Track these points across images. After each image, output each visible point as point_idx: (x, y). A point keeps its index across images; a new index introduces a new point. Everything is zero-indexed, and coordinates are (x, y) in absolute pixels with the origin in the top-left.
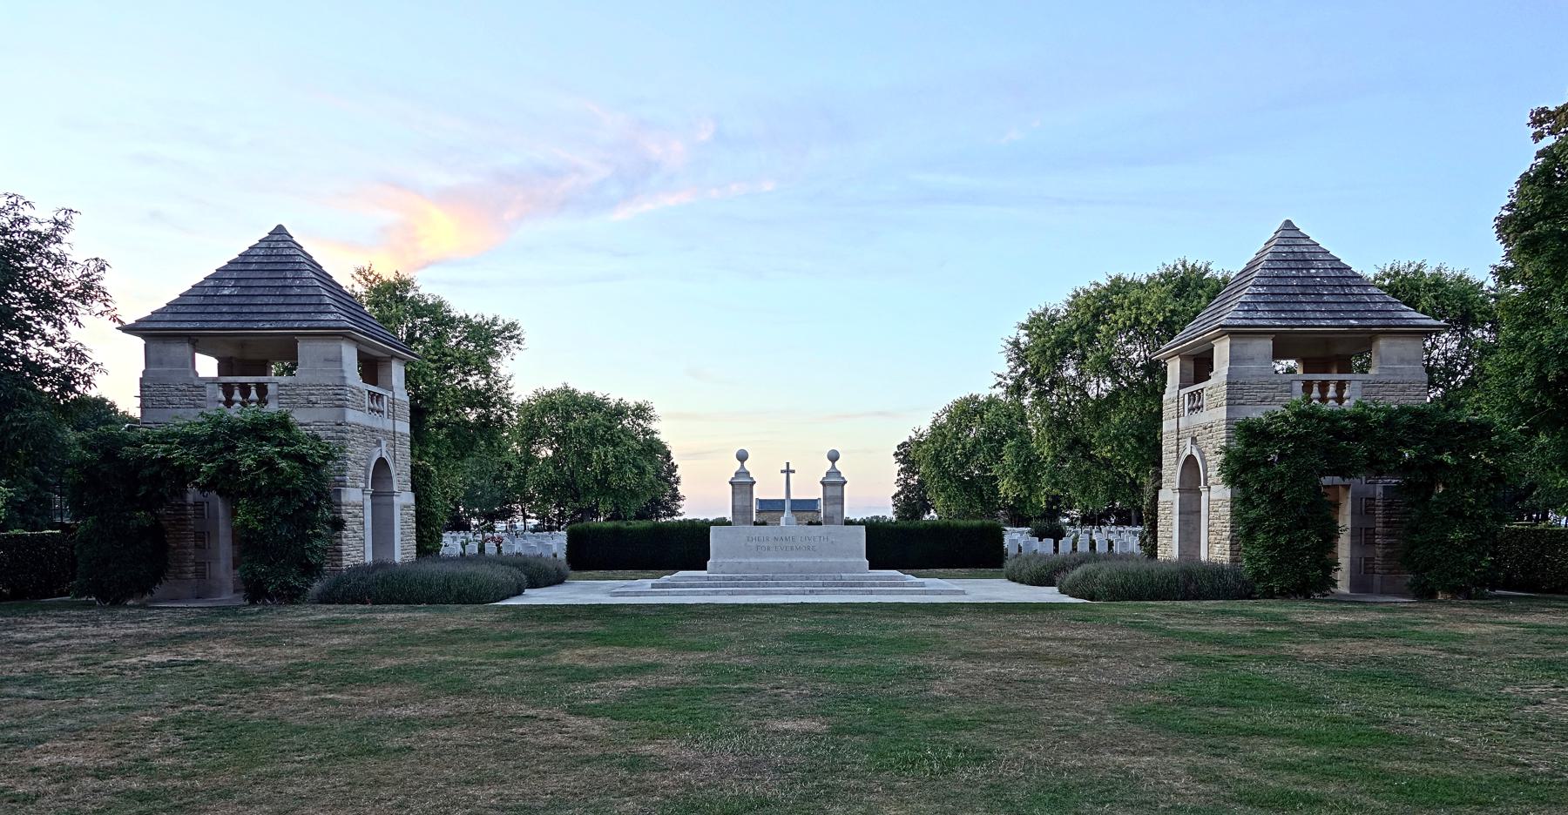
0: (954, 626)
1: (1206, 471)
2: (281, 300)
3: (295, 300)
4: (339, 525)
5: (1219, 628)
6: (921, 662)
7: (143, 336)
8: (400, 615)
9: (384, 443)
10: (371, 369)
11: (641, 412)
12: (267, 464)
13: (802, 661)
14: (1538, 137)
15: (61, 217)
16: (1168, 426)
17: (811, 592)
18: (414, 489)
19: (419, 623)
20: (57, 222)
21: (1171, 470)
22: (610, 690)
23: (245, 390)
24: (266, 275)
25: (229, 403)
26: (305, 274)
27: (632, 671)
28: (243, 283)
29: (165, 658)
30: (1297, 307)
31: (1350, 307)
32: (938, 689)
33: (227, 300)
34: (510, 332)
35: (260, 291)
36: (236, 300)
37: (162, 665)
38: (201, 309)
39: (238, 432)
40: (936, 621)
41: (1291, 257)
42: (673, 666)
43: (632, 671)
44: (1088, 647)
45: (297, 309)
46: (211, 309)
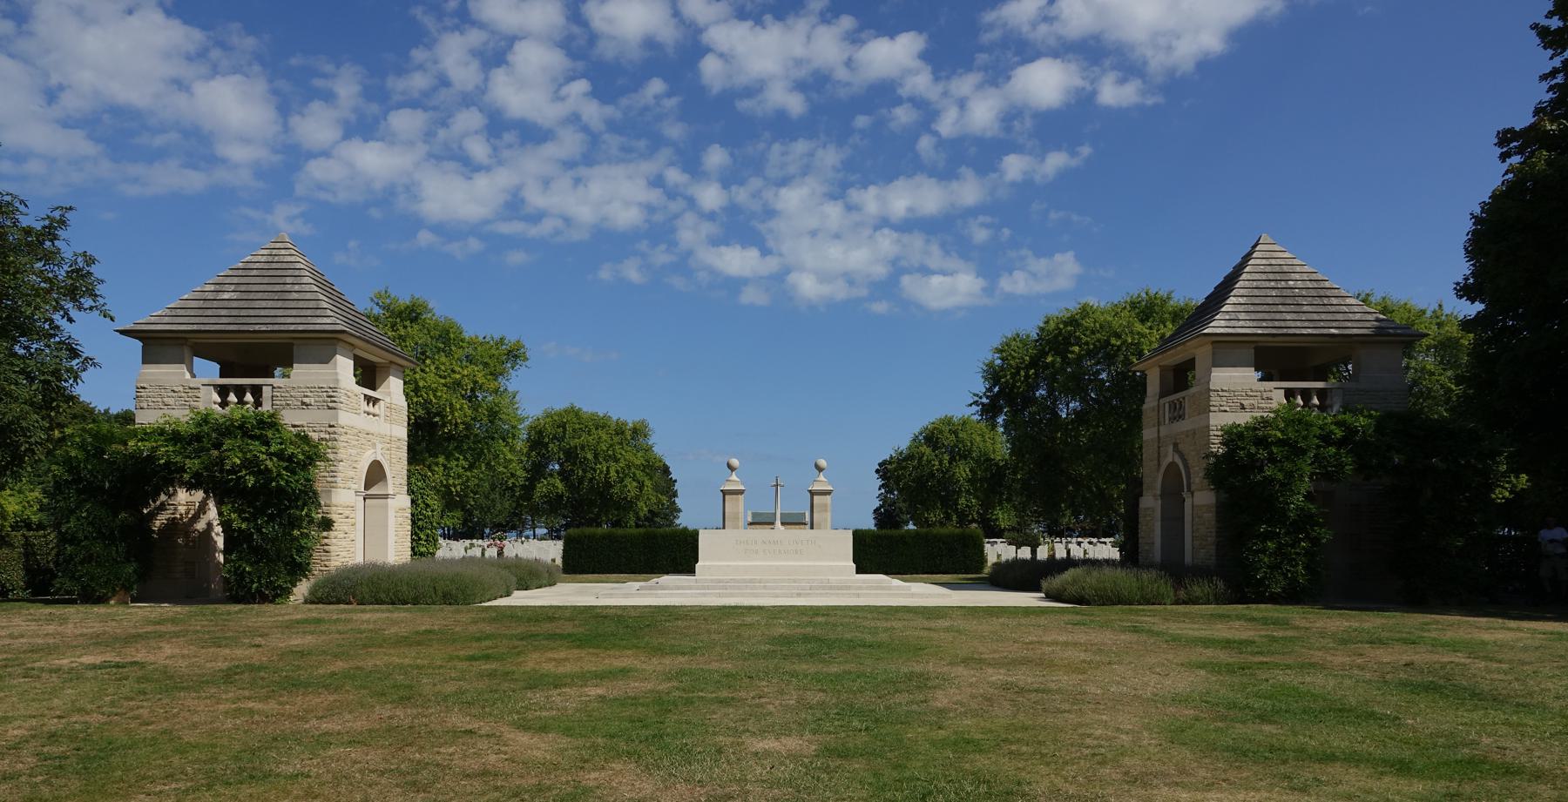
0: (947, 630)
1: (1189, 478)
2: (279, 304)
3: (293, 304)
4: (327, 524)
5: (1222, 631)
6: (918, 668)
7: (140, 339)
8: (378, 615)
9: (379, 446)
10: (369, 375)
11: (639, 431)
12: (251, 464)
13: (788, 667)
14: (1504, 157)
15: (57, 214)
16: (1148, 434)
17: (799, 595)
18: (410, 492)
19: (395, 623)
20: (52, 220)
21: (1153, 480)
22: (568, 700)
23: (240, 396)
24: (266, 280)
25: (224, 404)
26: (305, 280)
27: (601, 676)
28: (243, 288)
29: (98, 660)
30: (1278, 316)
31: (1329, 317)
32: (941, 700)
33: (226, 304)
34: (515, 355)
35: (259, 296)
36: (235, 304)
37: (94, 667)
38: (200, 312)
39: (227, 430)
40: (926, 624)
41: (1268, 269)
42: (648, 673)
43: (601, 676)
44: (1095, 653)
45: (294, 312)
46: (209, 312)
